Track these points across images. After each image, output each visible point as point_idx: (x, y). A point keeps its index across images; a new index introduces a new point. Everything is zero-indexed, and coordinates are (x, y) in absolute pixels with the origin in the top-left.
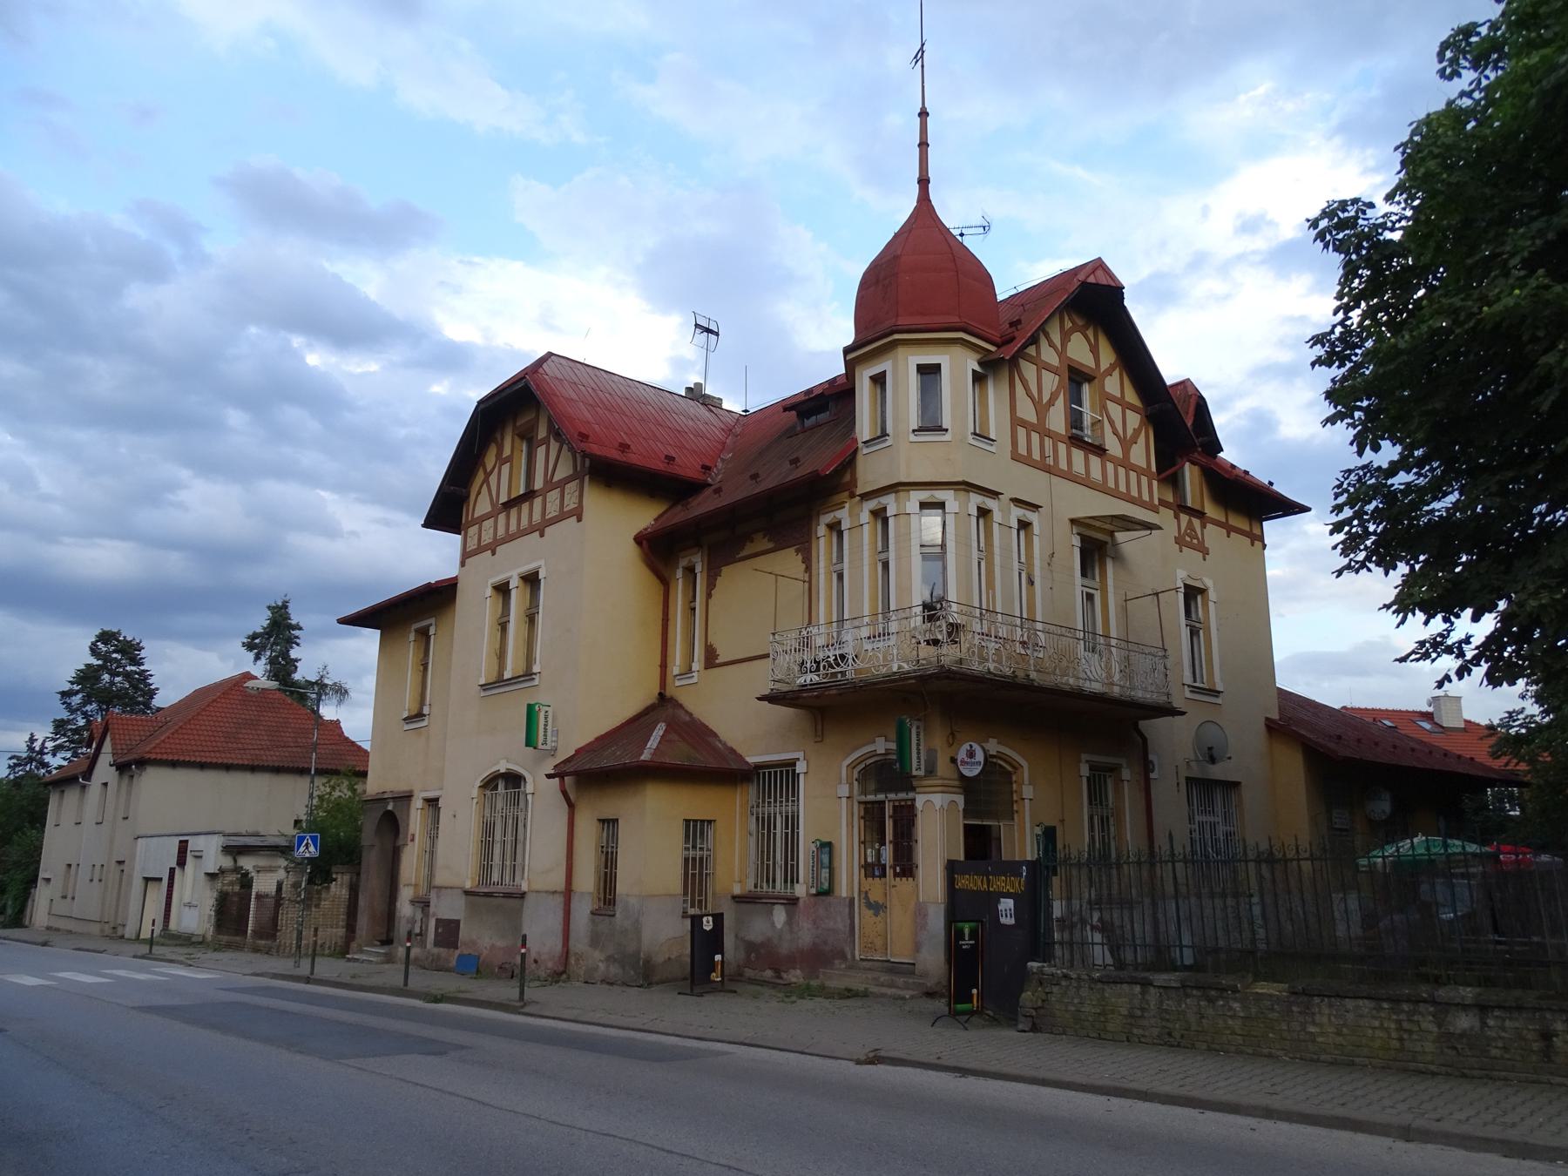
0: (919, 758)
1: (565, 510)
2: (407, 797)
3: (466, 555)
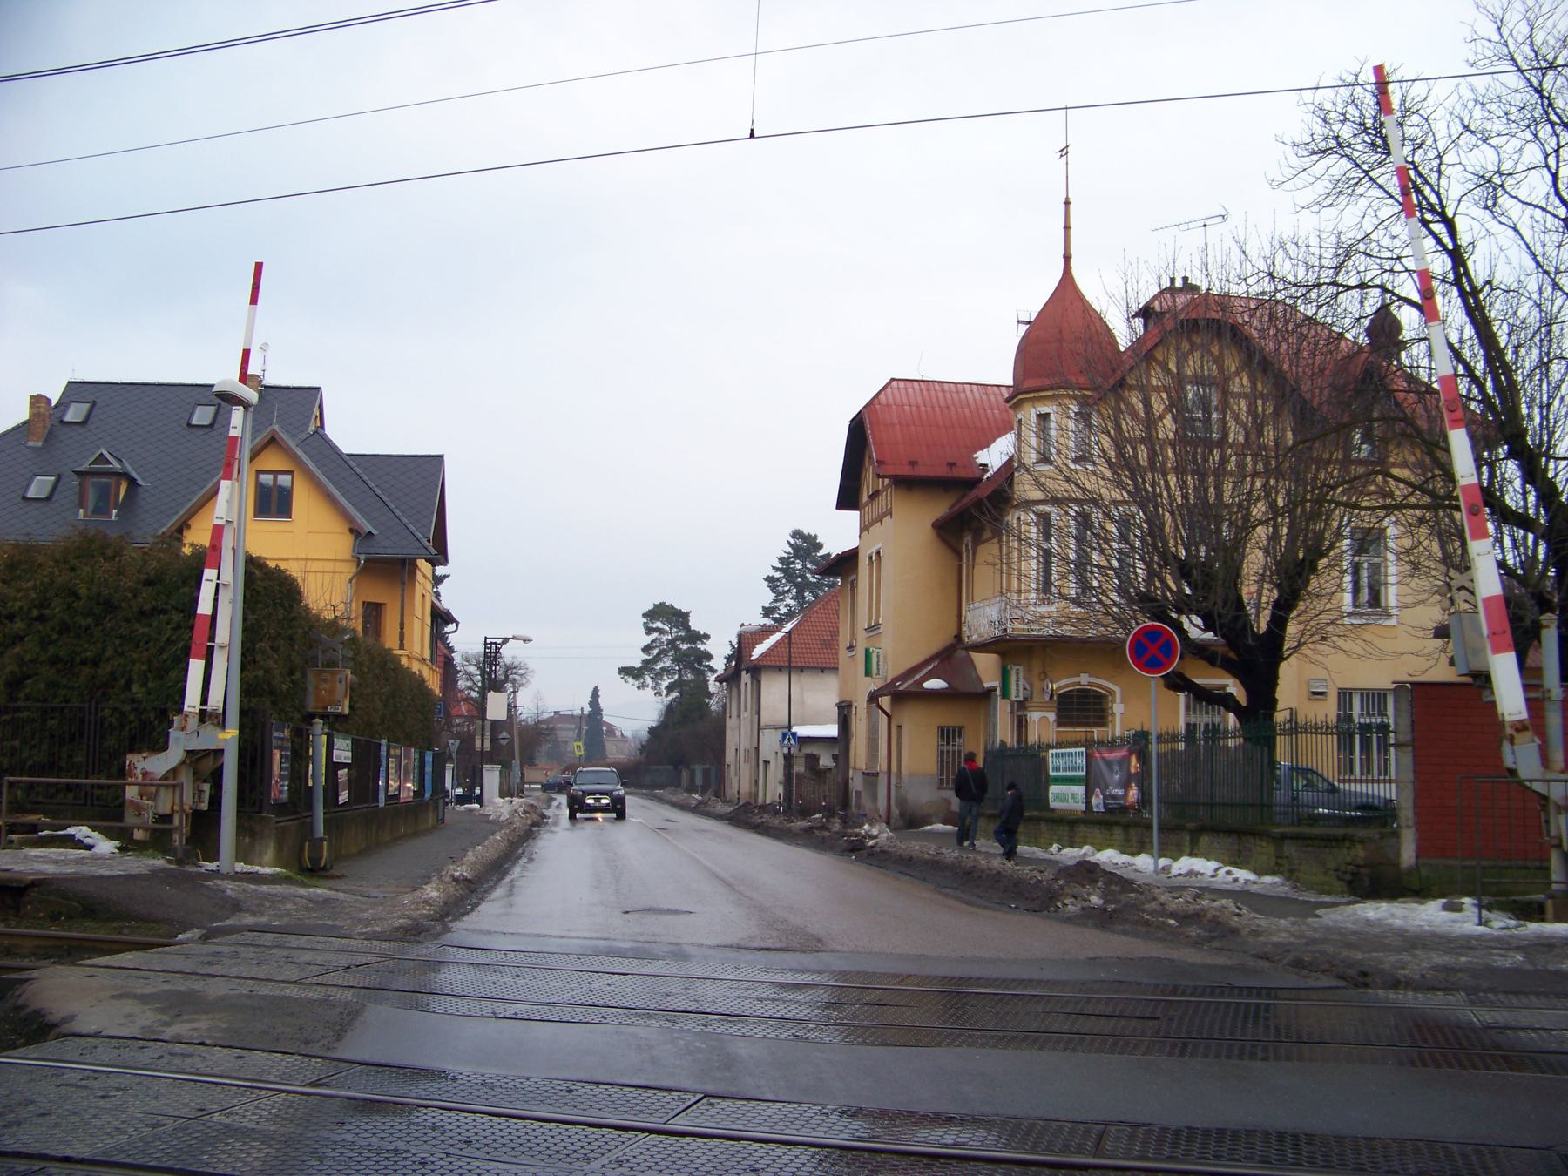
3: (864, 528)
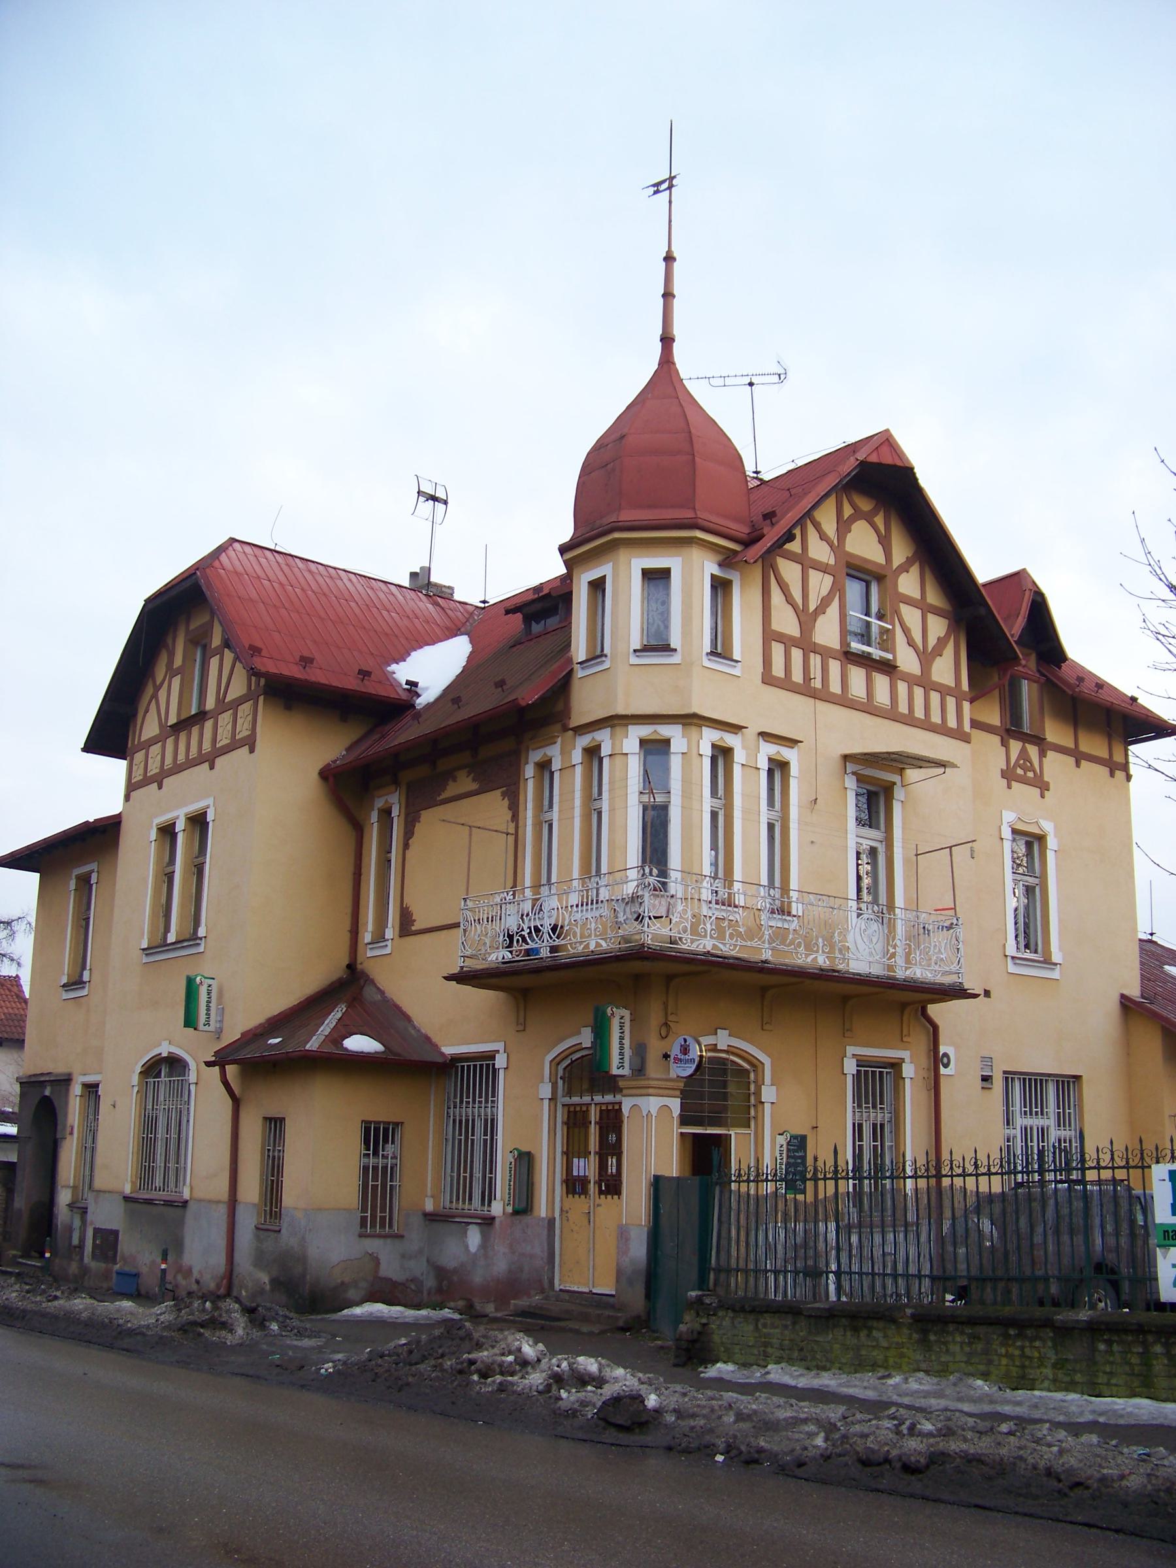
0: (621, 1054)
1: (237, 737)
2: (65, 1081)
3: (131, 787)
